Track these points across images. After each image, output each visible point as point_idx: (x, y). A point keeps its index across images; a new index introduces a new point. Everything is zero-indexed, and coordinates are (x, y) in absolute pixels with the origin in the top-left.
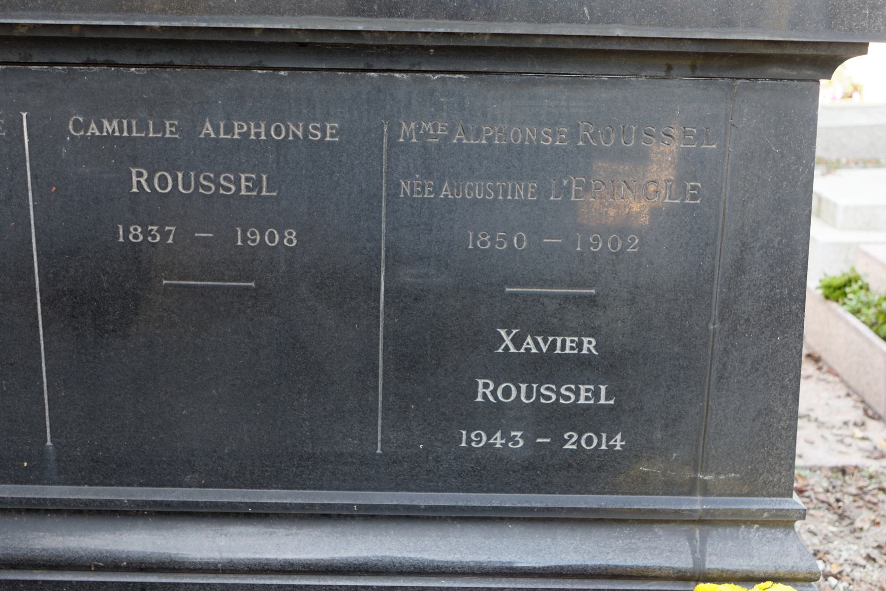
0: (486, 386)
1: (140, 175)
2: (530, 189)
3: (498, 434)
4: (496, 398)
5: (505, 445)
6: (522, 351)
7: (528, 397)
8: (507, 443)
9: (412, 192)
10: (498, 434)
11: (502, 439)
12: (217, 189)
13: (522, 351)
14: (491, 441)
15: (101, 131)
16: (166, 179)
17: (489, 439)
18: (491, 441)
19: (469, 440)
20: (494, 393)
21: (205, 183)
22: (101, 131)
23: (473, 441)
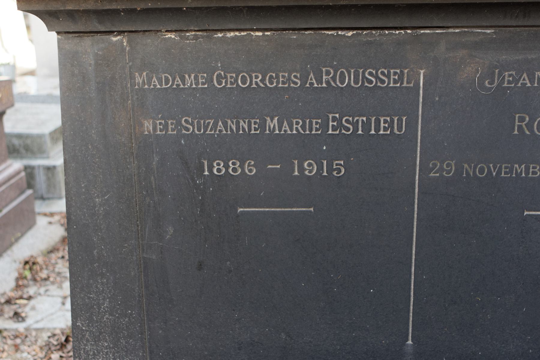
6: (152, 87)
13: (152, 87)
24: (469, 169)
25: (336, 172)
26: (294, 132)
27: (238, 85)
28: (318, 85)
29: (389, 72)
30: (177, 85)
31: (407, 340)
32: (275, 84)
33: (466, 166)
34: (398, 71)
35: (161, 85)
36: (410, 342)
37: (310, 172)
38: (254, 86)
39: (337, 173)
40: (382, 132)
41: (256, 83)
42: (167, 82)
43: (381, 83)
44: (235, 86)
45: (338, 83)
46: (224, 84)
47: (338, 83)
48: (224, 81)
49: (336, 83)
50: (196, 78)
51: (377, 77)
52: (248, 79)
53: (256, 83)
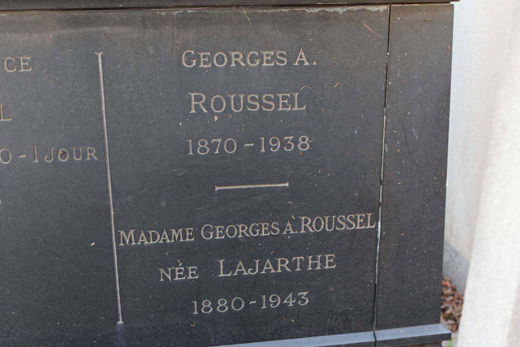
0: (243, 228)
1: (237, 56)
2: (188, 234)
3: (290, 296)
4: (249, 234)
5: (296, 304)
6: (139, 243)
7: (330, 228)
8: (297, 301)
9: (173, 276)
10: (290, 296)
11: (293, 300)
12: (261, 98)
13: (139, 243)
14: (285, 302)
15: (276, 269)
16: (253, 233)
17: (282, 300)
18: (285, 302)
19: (268, 302)
20: (248, 231)
21: (251, 102)
22: (276, 269)
23: (271, 303)
24: (165, 273)
25: (300, 301)
26: (279, 271)
27: (226, 236)
28: (294, 231)
29: (356, 217)
30: (163, 240)
31: (118, 320)
32: (258, 234)
33: (162, 271)
34: (364, 215)
35: (149, 240)
36: (121, 322)
37: (275, 304)
38: (240, 236)
39: (301, 303)
40: (327, 267)
41: (243, 234)
42: (154, 239)
43: (274, 232)
44: (223, 237)
45: (251, 233)
46: (211, 237)
47: (251, 233)
48: (212, 233)
49: (249, 234)
50: (184, 232)
51: (347, 223)
52: (236, 229)
53: (243, 234)
